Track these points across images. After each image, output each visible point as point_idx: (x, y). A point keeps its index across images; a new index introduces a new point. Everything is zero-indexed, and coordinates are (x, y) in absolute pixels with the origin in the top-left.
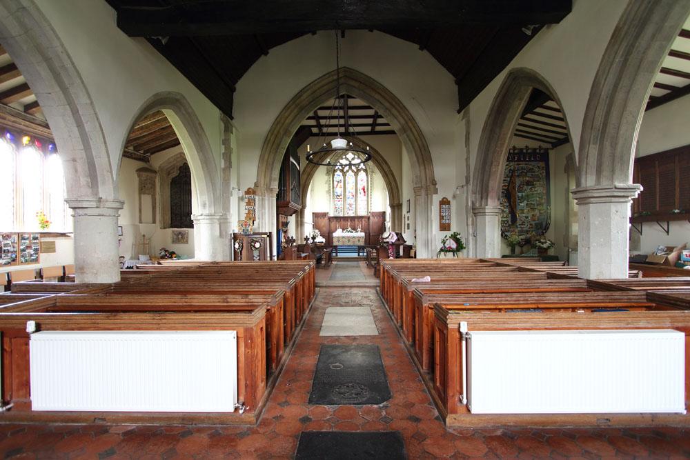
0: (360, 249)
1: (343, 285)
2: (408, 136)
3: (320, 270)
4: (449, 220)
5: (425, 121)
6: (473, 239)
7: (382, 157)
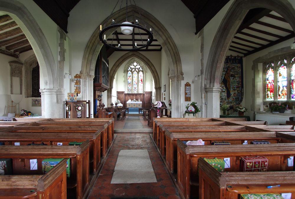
0: (140, 110)
1: (131, 131)
2: (168, 47)
3: (119, 121)
4: (190, 95)
5: (177, 38)
6: (204, 106)
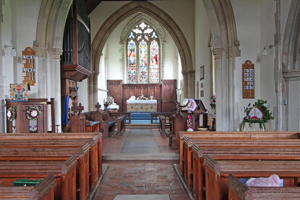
0: (153, 116)
6: (283, 108)
7: (175, 23)
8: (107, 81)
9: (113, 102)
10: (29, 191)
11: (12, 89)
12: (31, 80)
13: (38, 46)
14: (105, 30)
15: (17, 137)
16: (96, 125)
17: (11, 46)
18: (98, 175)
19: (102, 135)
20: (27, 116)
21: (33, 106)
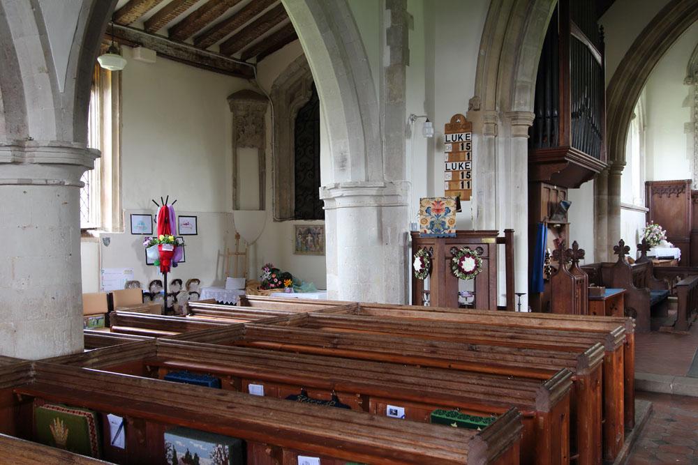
8: (647, 184)
9: (662, 239)
10: (468, 439)
11: (424, 209)
12: (463, 187)
13: (479, 110)
14: (643, 52)
15: (434, 316)
16: (617, 297)
17: (423, 116)
18: (625, 427)
19: (634, 325)
20: (453, 270)
21: (467, 248)
